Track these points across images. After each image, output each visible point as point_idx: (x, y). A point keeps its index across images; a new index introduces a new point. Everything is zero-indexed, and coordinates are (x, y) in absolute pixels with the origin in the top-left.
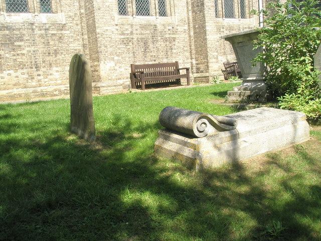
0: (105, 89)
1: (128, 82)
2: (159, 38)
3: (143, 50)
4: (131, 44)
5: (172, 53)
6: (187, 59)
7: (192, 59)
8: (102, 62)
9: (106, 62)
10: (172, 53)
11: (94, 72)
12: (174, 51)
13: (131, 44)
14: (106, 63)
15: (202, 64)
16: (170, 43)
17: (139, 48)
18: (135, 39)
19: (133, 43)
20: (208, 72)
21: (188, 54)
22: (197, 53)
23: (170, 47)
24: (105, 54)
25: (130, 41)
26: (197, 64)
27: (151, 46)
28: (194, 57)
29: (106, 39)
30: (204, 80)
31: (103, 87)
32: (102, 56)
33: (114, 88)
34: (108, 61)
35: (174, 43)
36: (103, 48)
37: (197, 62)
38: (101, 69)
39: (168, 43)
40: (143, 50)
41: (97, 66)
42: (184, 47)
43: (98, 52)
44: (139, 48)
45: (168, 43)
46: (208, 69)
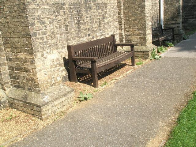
0: (50, 106)
1: (63, 72)
2: (92, 4)
3: (76, 21)
4: (62, 13)
5: (105, 24)
6: (117, 30)
7: (121, 29)
8: (39, 55)
9: (45, 52)
10: (105, 24)
11: (17, 69)
12: (106, 21)
13: (62, 13)
14: (45, 55)
15: (134, 35)
16: (102, 10)
17: (71, 18)
18: (67, 6)
19: (64, 12)
20: (145, 46)
21: (117, 24)
22: (128, 21)
23: (103, 15)
24: (42, 38)
25: (61, 9)
26: (127, 35)
27: (84, 14)
28: (123, 27)
29: (42, 7)
30: (140, 55)
31: (47, 104)
32: (37, 44)
33: (63, 99)
34: (49, 51)
35: (106, 10)
36: (38, 25)
37: (126, 33)
38: (38, 69)
39: (100, 11)
40: (76, 21)
41: (25, 60)
42: (114, 15)
43: (28, 35)
44: (71, 18)
45: (100, 11)
46: (145, 43)
